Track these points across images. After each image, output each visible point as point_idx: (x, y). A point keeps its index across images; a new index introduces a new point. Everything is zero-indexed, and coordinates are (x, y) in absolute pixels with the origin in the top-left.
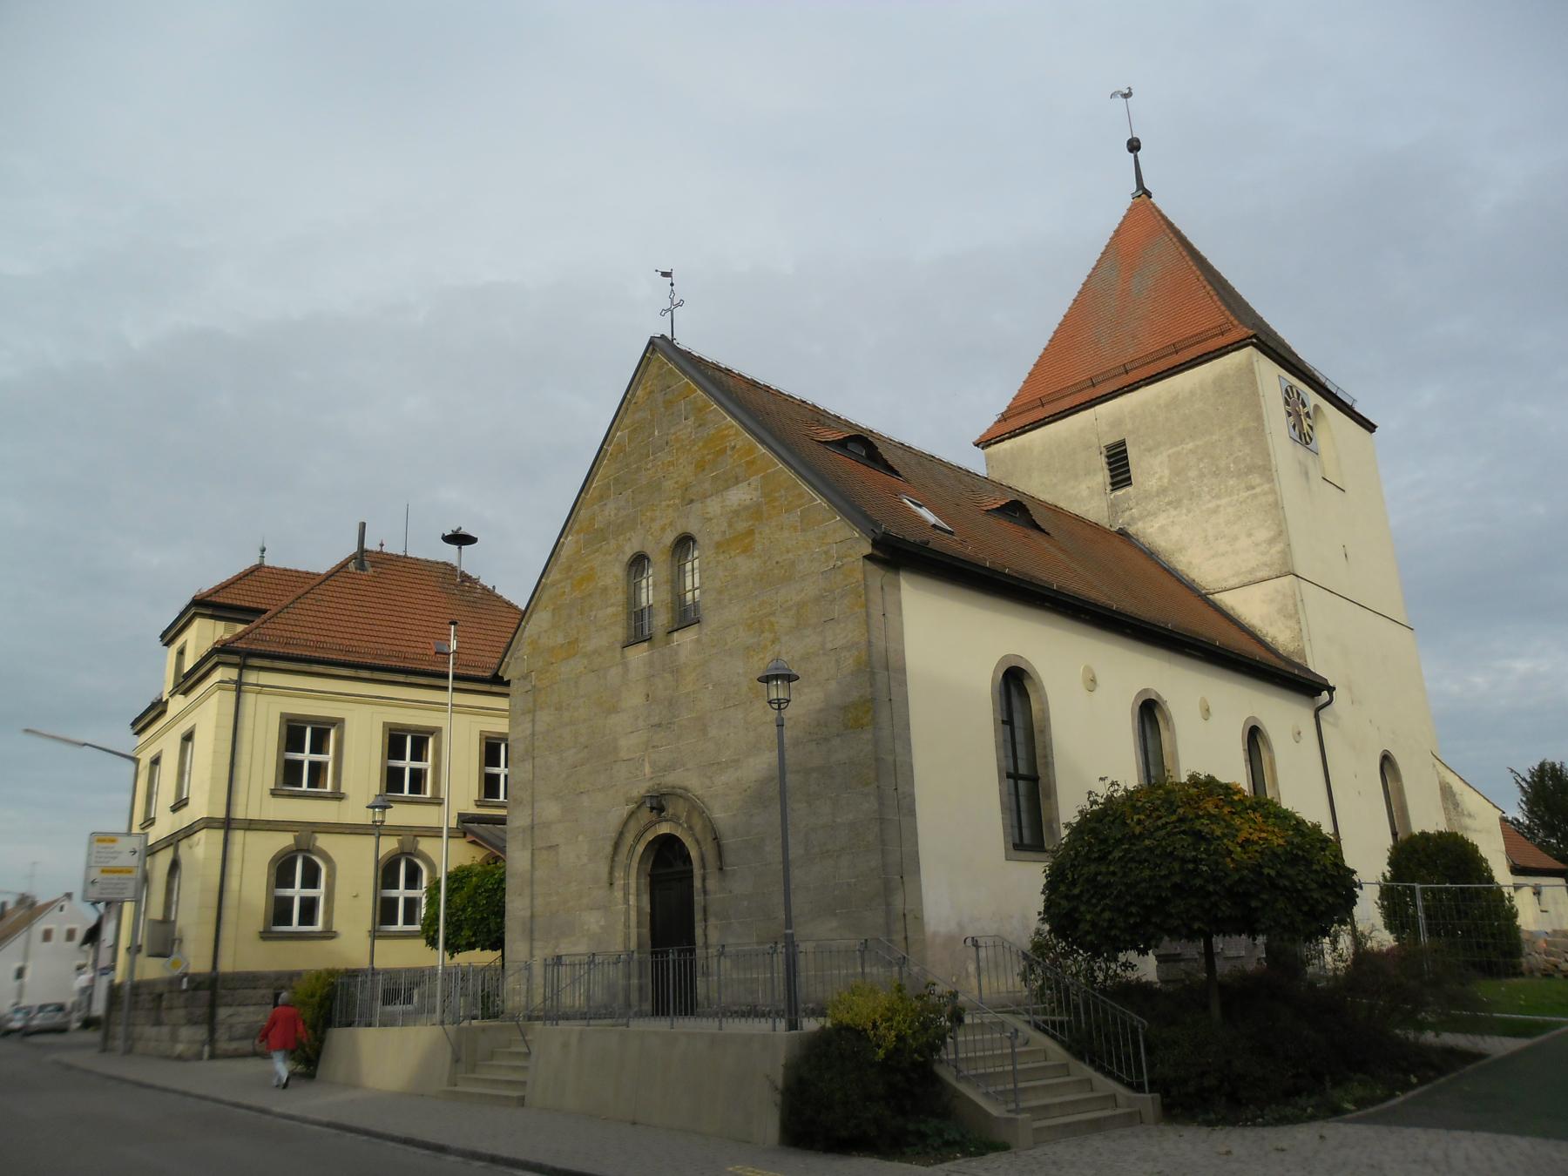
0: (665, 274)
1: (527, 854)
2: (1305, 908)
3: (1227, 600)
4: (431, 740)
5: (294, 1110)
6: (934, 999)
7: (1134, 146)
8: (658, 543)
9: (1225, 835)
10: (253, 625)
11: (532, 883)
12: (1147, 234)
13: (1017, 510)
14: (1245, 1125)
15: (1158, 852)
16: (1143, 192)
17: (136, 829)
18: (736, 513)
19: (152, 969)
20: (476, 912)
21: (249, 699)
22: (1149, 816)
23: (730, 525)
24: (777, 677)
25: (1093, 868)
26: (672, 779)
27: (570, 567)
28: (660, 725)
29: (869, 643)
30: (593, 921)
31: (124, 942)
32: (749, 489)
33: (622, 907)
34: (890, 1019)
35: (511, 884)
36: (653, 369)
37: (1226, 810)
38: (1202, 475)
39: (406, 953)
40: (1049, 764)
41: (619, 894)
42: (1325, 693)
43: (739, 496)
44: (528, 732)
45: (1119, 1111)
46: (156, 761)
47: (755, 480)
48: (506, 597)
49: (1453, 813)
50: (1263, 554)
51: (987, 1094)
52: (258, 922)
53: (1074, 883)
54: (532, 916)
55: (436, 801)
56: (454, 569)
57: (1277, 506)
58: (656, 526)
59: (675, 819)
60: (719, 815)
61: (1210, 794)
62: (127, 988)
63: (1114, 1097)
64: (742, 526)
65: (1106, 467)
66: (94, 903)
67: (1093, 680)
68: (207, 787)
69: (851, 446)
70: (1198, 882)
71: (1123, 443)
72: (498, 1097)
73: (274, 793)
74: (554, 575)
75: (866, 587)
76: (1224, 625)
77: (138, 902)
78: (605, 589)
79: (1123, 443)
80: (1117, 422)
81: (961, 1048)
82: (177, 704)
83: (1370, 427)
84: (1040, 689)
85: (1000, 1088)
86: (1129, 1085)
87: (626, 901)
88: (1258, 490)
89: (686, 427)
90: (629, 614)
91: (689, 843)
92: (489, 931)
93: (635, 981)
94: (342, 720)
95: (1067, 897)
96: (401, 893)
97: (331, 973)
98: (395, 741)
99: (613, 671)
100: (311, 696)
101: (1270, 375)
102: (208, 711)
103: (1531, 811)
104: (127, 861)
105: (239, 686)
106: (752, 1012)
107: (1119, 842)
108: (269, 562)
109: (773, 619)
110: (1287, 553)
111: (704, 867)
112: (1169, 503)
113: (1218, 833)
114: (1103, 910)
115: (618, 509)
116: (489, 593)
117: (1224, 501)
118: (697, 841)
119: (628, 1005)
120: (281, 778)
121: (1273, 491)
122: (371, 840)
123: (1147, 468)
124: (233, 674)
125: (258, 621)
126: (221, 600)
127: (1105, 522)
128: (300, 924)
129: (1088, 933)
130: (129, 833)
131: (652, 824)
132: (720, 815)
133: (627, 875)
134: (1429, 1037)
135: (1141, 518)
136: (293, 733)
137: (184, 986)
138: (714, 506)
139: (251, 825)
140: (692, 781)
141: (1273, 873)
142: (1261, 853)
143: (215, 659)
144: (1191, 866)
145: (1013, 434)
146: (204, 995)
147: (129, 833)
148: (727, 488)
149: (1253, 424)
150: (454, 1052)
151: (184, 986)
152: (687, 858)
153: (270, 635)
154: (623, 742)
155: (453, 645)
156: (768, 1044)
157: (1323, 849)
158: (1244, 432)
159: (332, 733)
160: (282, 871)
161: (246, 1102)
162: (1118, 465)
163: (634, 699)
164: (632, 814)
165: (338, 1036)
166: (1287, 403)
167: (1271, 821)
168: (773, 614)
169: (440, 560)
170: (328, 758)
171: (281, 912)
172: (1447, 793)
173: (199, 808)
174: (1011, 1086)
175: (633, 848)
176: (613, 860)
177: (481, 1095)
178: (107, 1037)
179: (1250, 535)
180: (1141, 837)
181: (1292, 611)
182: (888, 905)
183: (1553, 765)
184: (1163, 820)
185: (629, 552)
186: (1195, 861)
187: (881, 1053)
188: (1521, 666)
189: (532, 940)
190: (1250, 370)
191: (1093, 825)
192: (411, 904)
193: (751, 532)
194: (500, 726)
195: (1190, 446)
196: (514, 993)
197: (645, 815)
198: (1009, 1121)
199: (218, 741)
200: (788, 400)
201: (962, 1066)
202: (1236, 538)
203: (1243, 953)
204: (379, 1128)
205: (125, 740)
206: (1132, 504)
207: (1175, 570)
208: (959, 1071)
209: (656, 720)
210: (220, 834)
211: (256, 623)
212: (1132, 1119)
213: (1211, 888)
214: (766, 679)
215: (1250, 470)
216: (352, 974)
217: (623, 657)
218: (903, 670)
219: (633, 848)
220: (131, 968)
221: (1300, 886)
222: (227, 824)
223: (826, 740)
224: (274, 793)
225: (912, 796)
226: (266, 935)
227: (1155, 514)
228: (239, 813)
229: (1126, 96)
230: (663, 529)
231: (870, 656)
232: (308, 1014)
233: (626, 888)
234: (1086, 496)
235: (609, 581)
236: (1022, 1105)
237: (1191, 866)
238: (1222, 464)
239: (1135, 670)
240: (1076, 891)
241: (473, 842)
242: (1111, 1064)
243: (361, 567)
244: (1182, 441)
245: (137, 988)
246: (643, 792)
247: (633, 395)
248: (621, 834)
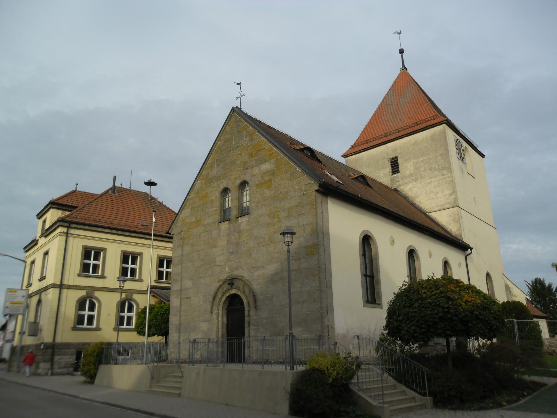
0: (238, 84)
1: (179, 300)
2: (489, 327)
3: (434, 215)
4: (139, 258)
5: (88, 396)
6: (350, 359)
7: (401, 51)
8: (233, 183)
9: (459, 298)
10: (73, 212)
11: (180, 311)
12: (405, 83)
13: (363, 179)
14: (467, 410)
15: (433, 304)
16: (404, 68)
17: (24, 288)
18: (265, 173)
19: (29, 341)
20: (158, 321)
21: (71, 239)
22: (428, 291)
23: (262, 178)
24: (288, 233)
25: (407, 310)
27: (198, 193)
28: (232, 253)
29: (317, 223)
30: (204, 326)
31: (18, 330)
32: (271, 163)
33: (215, 321)
34: (333, 366)
35: (172, 311)
36: (233, 119)
37: (458, 289)
38: (425, 170)
39: (129, 337)
40: (378, 271)
41: (215, 316)
42: (469, 250)
43: (266, 167)
44: (180, 254)
45: (417, 404)
46: (33, 262)
47: (273, 161)
48: (167, 206)
49: (509, 295)
50: (447, 199)
51: (370, 397)
52: (71, 324)
53: (399, 315)
54: (180, 324)
55: (140, 280)
56: (148, 195)
57: (453, 182)
58: (233, 178)
59: (238, 288)
60: (255, 287)
61: (451, 282)
62: (19, 348)
63: (414, 398)
64: (267, 178)
65: (390, 166)
66: (6, 315)
67: (393, 241)
68: (53, 271)
69: (305, 151)
70: (449, 316)
71: (397, 157)
72: (170, 393)
73: (79, 275)
74: (192, 195)
75: (316, 202)
76: (433, 224)
77: (24, 315)
78: (212, 201)
79: (397, 157)
80: (395, 150)
81: (360, 377)
82: (42, 241)
83: (483, 156)
84: (375, 243)
85: (376, 393)
86: (420, 394)
88: (446, 176)
89: (245, 141)
90: (221, 211)
91: (243, 297)
92: (161, 329)
93: (220, 349)
94: (106, 249)
95: (396, 321)
96: (126, 314)
97: (102, 344)
98: (125, 257)
99: (215, 232)
100: (94, 239)
101: (450, 133)
102: (55, 244)
103: (531, 295)
104: (20, 299)
105: (67, 235)
106: (282, 363)
107: (417, 300)
108: (79, 189)
109: (278, 213)
110: (456, 199)
111: (249, 306)
112: (413, 180)
113: (456, 297)
114: (411, 326)
115: (218, 171)
116: (161, 204)
117: (433, 180)
118: (246, 297)
119: (218, 359)
120: (82, 270)
121: (452, 176)
122: (119, 294)
123: (405, 167)
124: (65, 230)
125: (75, 211)
126: (61, 202)
127: (389, 186)
128: (87, 325)
129: (405, 335)
130: (21, 289)
132: (255, 287)
133: (218, 309)
134: (526, 377)
135: (403, 185)
136: (87, 253)
137: (42, 347)
138: (256, 171)
139: (70, 287)
140: (244, 273)
141: (478, 313)
142: (473, 306)
143: (58, 224)
144: (446, 310)
145: (356, 153)
146: (50, 351)
147: (21, 289)
148: (261, 164)
149: (444, 152)
150: (151, 375)
151: (42, 347)
152: (242, 303)
153: (79, 216)
154: (218, 259)
155: (154, 220)
156: (283, 376)
157: (494, 305)
158: (442, 155)
159: (102, 253)
160: (81, 305)
161: (69, 393)
162: (395, 165)
163: (222, 242)
164: (221, 286)
165: (103, 368)
166: (456, 145)
167: (474, 294)
168: (279, 211)
169: (143, 191)
170: (100, 263)
171: (80, 320)
172: (507, 288)
173: (52, 278)
174: (381, 393)
175: (221, 298)
176: (213, 303)
177: (163, 393)
178: (10, 366)
179: (443, 192)
180: (425, 298)
181: (458, 220)
182: (322, 322)
183: (540, 280)
184: (435, 292)
185: (222, 187)
186: (448, 308)
187: (331, 379)
188: (514, 246)
189: (180, 333)
190: (444, 132)
191: (405, 293)
192: (129, 319)
193: (270, 181)
194: (169, 253)
195: (422, 159)
196: (172, 352)
197: (226, 286)
198: (380, 407)
199: (59, 255)
200: (281, 133)
201: (360, 385)
202: (437, 193)
204: (124, 405)
205: (22, 255)
206: (399, 179)
207: (415, 204)
208: (359, 387)
209: (231, 250)
210: (57, 290)
211: (73, 211)
212: (423, 407)
213: (454, 318)
214: (283, 234)
215: (443, 168)
216: (110, 344)
217: (219, 227)
218: (328, 234)
219: (221, 298)
220: (21, 340)
221: (487, 319)
222: (61, 286)
223: (299, 259)
224: (79, 275)
225: (331, 281)
226: (74, 329)
227: (408, 184)
228: (66, 282)
229: (399, 33)
230: (236, 179)
231: (317, 228)
232: (92, 359)
233: (218, 313)
234: (383, 175)
235: (213, 198)
236: (386, 400)
237: (446, 310)
238: (433, 166)
239: (407, 238)
240: (400, 318)
241: (153, 296)
242: (413, 385)
243: (114, 192)
244: (419, 158)
245: (23, 348)
246: (225, 277)
247: (225, 129)
248: (216, 293)
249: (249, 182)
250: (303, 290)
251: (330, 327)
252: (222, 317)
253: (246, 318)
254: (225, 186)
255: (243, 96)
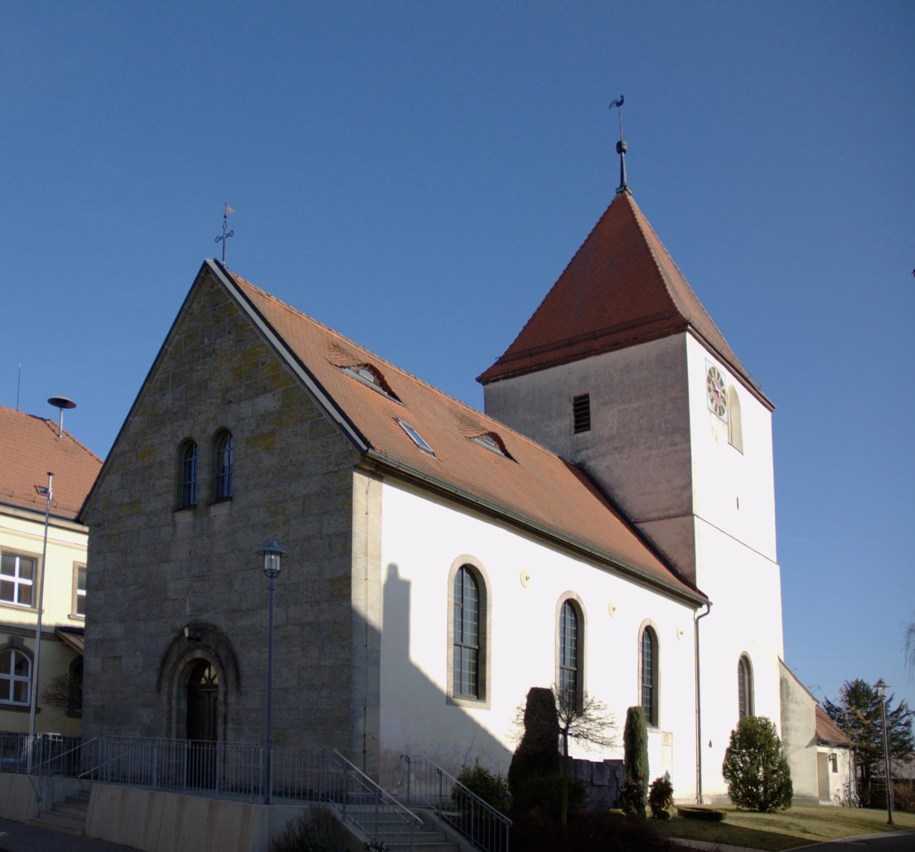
7: (620, 148)
23: (258, 426)
26: (205, 618)
28: (198, 577)
41: (165, 698)
59: (207, 647)
65: (572, 412)
78: (162, 463)
87: (170, 703)
88: (679, 447)
131: (191, 650)
138: (246, 409)
140: (221, 622)
148: (257, 395)
166: (709, 380)
168: (286, 501)
175: (175, 666)
179: (669, 481)
195: (635, 405)
203: (607, 783)
217: (173, 517)
225: (378, 651)
229: (619, 104)
233: (170, 694)
247: (190, 307)
249: (233, 432)
250: (323, 663)
251: (368, 738)
252: (178, 700)
253: (221, 708)
254: (187, 435)
255: (229, 235)
